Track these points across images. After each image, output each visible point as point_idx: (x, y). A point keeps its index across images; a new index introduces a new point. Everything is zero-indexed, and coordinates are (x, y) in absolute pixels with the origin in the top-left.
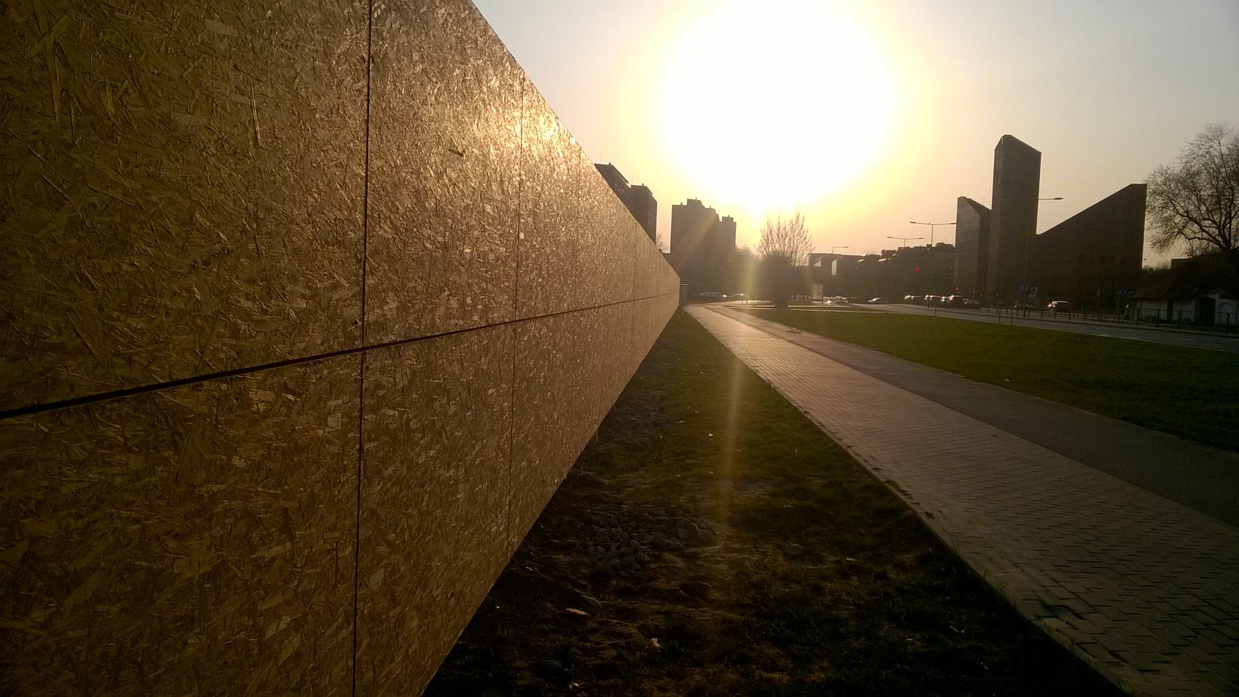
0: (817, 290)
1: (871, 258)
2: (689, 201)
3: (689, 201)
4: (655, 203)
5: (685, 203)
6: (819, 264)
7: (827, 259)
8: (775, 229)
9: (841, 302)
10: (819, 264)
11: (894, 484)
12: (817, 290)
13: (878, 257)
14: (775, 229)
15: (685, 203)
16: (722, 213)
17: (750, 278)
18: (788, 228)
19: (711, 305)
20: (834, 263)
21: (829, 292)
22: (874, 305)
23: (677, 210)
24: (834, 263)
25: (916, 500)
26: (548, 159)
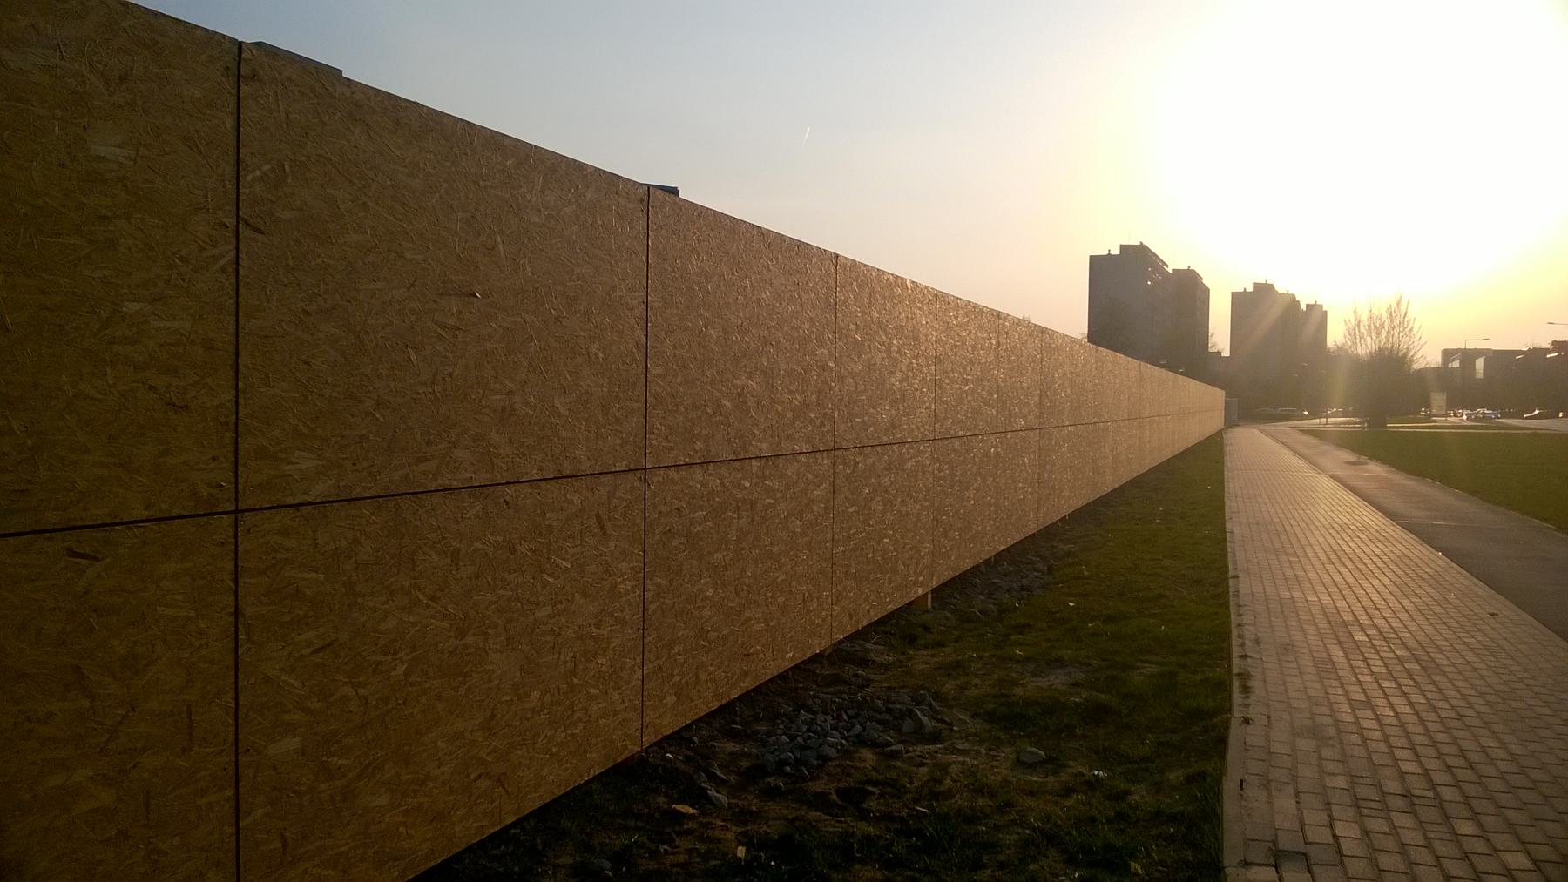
0: (1438, 400)
1: (1536, 354)
2: (1123, 247)
3: (1123, 247)
4: (1206, 291)
5: (1250, 289)
6: (1456, 364)
7: (1468, 356)
8: (1364, 318)
9: (1485, 417)
10: (1456, 364)
11: (1246, 690)
12: (1438, 400)
13: (1547, 351)
14: (1364, 318)
15: (1250, 289)
16: (1174, 261)
17: (1339, 384)
18: (1385, 315)
19: (1271, 427)
20: (1479, 364)
21: (1453, 404)
22: (1532, 422)
23: (1238, 300)
24: (1479, 364)
25: (1251, 712)
26: (1412, 361)
